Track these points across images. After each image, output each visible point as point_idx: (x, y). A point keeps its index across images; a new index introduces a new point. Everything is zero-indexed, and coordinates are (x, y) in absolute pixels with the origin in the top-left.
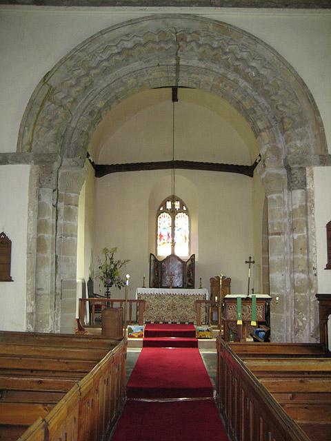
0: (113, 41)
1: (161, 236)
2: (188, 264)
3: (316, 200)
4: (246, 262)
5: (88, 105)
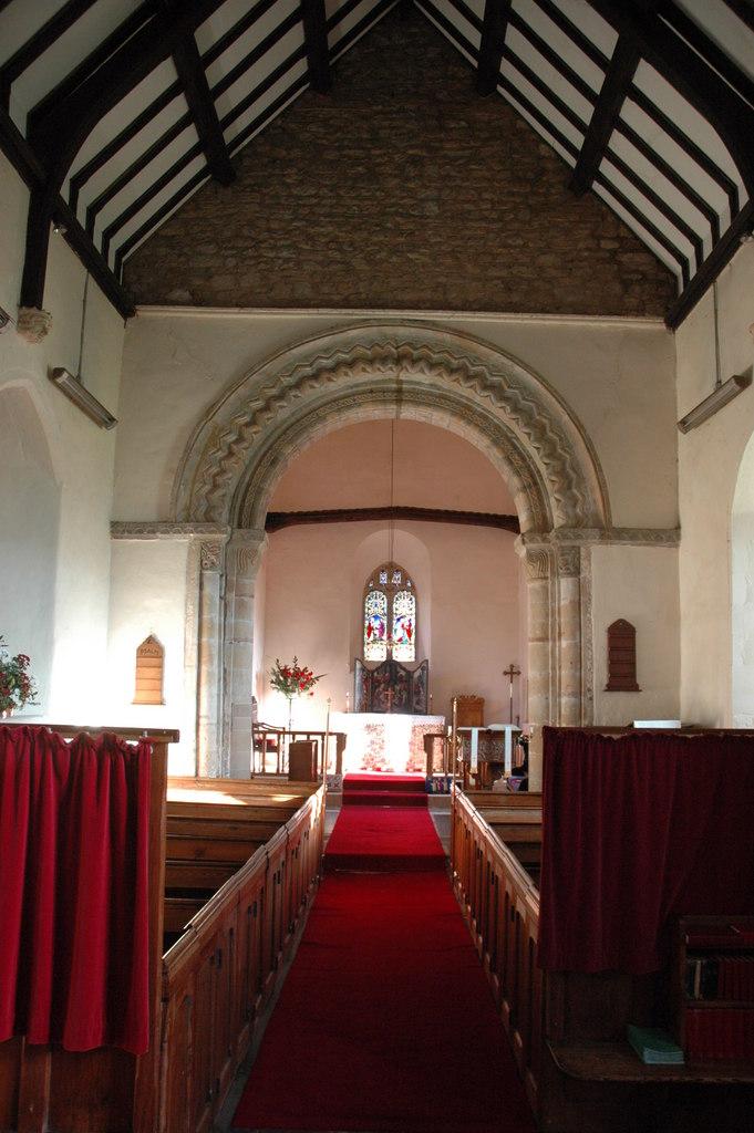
0: (306, 357)
1: (370, 629)
2: (416, 675)
3: (593, 593)
4: (506, 673)
5: (267, 452)
